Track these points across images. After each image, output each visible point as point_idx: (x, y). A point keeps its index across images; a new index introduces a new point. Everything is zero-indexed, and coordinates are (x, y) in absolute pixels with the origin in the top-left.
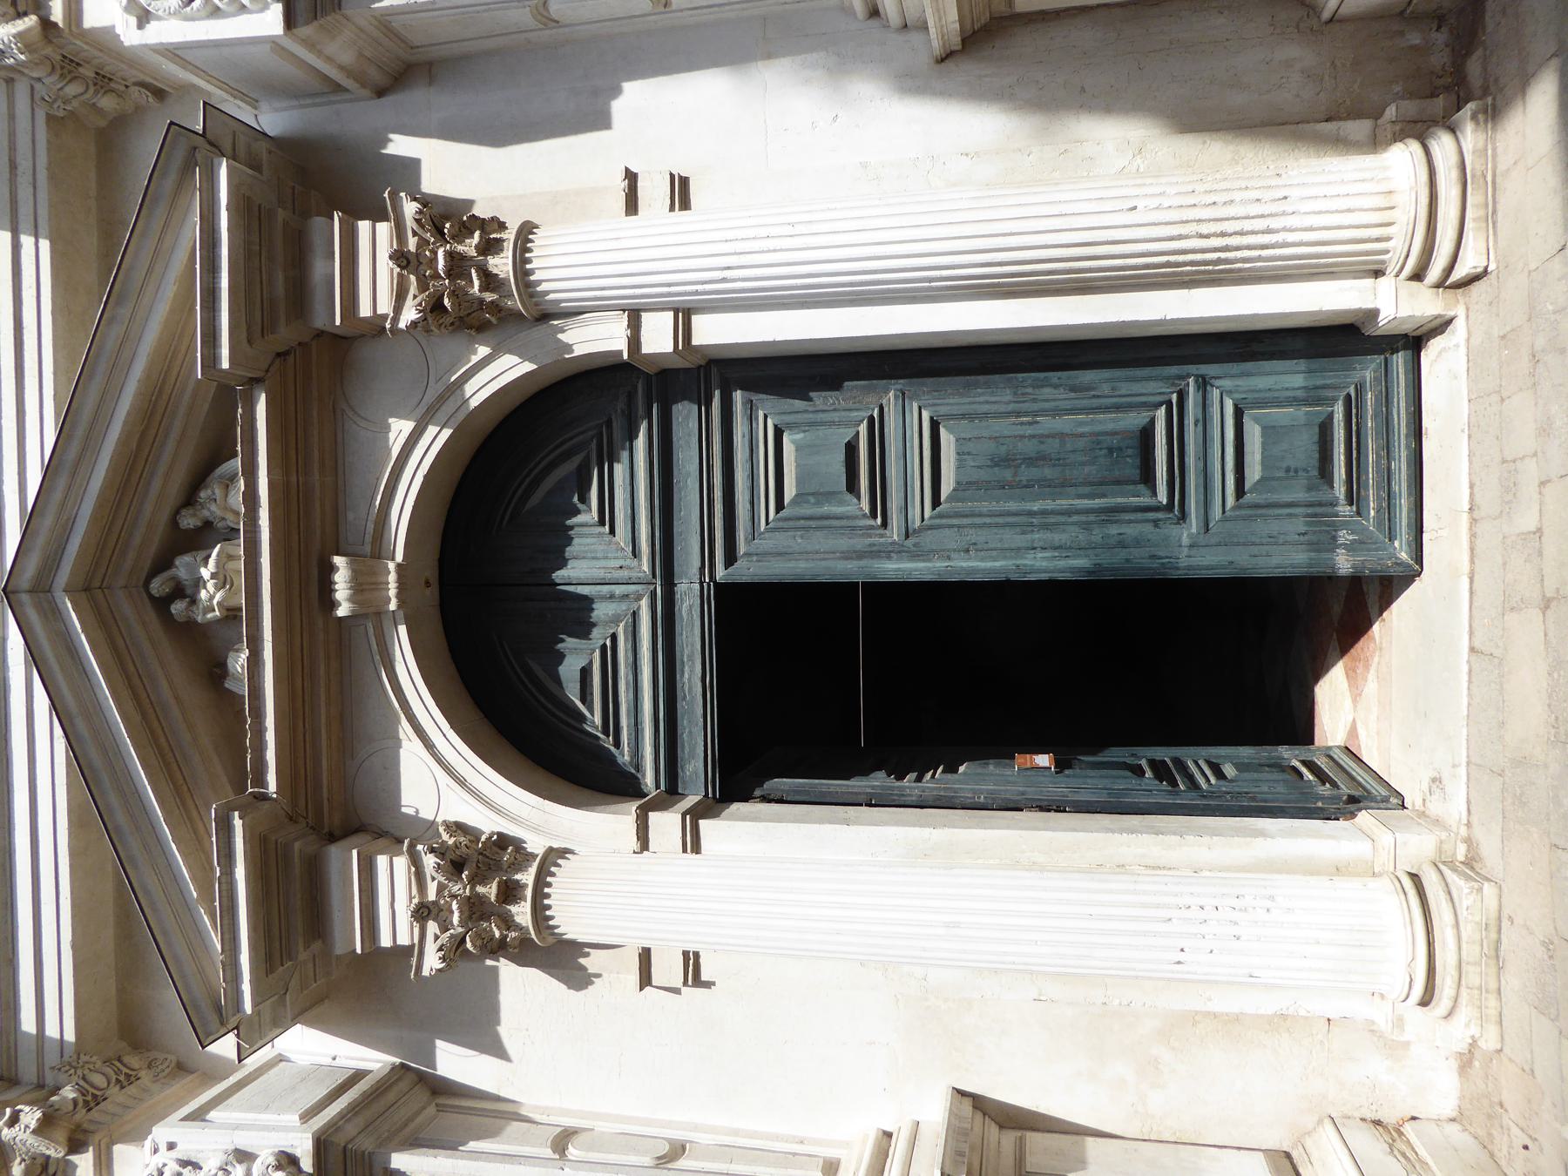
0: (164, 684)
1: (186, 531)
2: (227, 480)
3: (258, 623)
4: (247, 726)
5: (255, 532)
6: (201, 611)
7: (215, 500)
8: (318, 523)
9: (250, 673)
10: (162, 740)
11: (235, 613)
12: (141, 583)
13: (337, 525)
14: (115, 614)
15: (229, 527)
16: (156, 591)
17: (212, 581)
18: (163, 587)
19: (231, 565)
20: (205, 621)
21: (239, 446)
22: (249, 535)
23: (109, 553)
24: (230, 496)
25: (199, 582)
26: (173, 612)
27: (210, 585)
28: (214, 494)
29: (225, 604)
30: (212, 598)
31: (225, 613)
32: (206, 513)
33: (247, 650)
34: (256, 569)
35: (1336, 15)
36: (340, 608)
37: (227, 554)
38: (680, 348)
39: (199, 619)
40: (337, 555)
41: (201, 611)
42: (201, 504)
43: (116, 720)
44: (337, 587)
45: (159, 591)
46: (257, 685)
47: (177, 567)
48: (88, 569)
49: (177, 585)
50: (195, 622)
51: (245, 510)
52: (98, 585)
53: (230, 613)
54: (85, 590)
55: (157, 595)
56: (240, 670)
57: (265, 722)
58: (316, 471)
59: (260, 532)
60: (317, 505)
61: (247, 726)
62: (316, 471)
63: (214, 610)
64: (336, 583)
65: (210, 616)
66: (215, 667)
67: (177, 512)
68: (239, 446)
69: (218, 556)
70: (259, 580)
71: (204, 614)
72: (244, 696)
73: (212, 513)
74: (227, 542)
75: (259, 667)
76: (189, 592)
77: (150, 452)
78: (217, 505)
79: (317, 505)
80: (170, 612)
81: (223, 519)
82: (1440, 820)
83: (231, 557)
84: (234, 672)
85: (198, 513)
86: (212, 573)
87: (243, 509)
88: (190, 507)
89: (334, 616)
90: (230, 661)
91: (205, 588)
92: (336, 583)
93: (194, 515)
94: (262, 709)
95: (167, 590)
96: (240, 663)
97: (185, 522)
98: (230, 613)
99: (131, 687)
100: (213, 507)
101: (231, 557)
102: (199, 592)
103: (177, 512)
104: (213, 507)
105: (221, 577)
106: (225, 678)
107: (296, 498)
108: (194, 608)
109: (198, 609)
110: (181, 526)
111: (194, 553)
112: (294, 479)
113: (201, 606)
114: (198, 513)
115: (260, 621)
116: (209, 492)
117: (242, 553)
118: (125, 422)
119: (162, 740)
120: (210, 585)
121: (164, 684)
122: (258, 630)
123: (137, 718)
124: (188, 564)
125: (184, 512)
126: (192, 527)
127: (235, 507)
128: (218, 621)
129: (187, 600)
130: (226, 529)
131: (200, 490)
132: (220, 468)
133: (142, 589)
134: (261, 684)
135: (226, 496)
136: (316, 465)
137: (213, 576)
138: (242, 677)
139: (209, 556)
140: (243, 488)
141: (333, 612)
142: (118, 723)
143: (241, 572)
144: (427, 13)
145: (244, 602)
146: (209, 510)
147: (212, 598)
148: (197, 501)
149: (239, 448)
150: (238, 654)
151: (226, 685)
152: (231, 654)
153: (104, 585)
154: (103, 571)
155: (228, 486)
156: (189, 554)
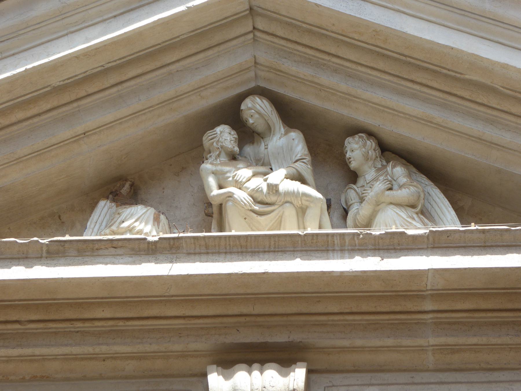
0: (109, 116)
1: (342, 145)
2: (424, 206)
3: (200, 253)
4: (35, 239)
5: (342, 250)
6: (219, 168)
7: (391, 189)
8: (359, 343)
9: (120, 244)
10: (20, 115)
11: (216, 215)
12: (262, 84)
13: (356, 370)
14: (216, 49)
15: (349, 206)
16: (250, 105)
17: (265, 188)
18: (257, 116)
19: (290, 213)
20: (203, 174)
21: (477, 227)
22: (337, 241)
23: (306, 40)
24: (398, 210)
25: (263, 165)
26: (218, 129)
27: (258, 183)
28: (401, 187)
29: (230, 203)
30: (239, 185)
31: (215, 203)
32: (370, 174)
33: (156, 239)
34: (284, 252)
35: (244, 167)
36: (221, 377)
37: (307, 207)
38: (255, 189)
39: (207, 166)
40: (309, 372)
41: (219, 168)
42: (384, 167)
43: (54, 54)
44: (256, 373)
45: (250, 109)
46: (101, 252)
47: (286, 133)
48: (284, 13)
49: (259, 134)
50: (201, 159)
51: (375, 237)
52: (260, 26)
53: (215, 210)
54: (251, 9)
55: (243, 107)
56: (126, 224)
57: (42, 265)
58: (442, 340)
59: (342, 258)
60: (390, 342)
61: (35, 239)
62: (442, 340)
63: (220, 187)
64: (262, 373)
65: (212, 181)
66: (132, 185)
67: (371, 134)
68: (477, 227)
69: (305, 195)
70: (266, 256)
71: (214, 173)
72: (82, 235)
73: (370, 183)
74: (325, 207)
75: (131, 255)
76: (248, 149)
77: (462, 98)
78: (383, 192)
79: (390, 342)
80: (218, 125)
81: (362, 200)
82: (46, 259)
83: (302, 212)
84: (122, 217)
85: (370, 163)
86: (277, 186)
87: (377, 233)
88: (378, 152)
89: (209, 368)
90: (139, 210)
91: (255, 175)
92: (262, 373)
93: (367, 158)
94: (62, 260)
95: (251, 121)
96: (136, 224)
97: (356, 146)
98: (215, 210)
99: (105, 72)
100: (379, 186)
101: (302, 212)
102: (248, 166)
103: (371, 134)
104: (379, 186)
105: (272, 199)
106: (114, 200)
107: (398, 308)
108: (224, 158)
109: (222, 164)
110: (349, 139)
111: (308, 158)
112: (429, 306)
113: (227, 169)
114: (370, 163)
115: (204, 257)
116: (403, 180)
117: (309, 231)
118: (505, 66)
119: (20, 115)
120: (258, 183)
121: (109, 116)
122: (189, 254)
123: (55, 81)
124: (291, 150)
125: (371, 144)
126: (348, 156)
127: (380, 218)
128: (202, 189)
129: (237, 149)
130: (347, 204)
131: (404, 165)
132: (442, 196)
133: (252, 85)
134: (101, 259)
135: (399, 205)
136: (451, 340)
137: (273, 188)
138: (114, 228)
139: (303, 181)
140: (410, 232)
141: (215, 366)
142: (48, 56)
143: (279, 229)
144: (351, 40)
145: (233, 233)
146: (376, 179)
147: (239, 185)
148: (388, 162)
149: (473, 227)
150: (151, 222)
151: (102, 203)
152: (151, 212)
153: (258, 34)
154: (280, 33)
155: (413, 206)
156: (306, 152)
